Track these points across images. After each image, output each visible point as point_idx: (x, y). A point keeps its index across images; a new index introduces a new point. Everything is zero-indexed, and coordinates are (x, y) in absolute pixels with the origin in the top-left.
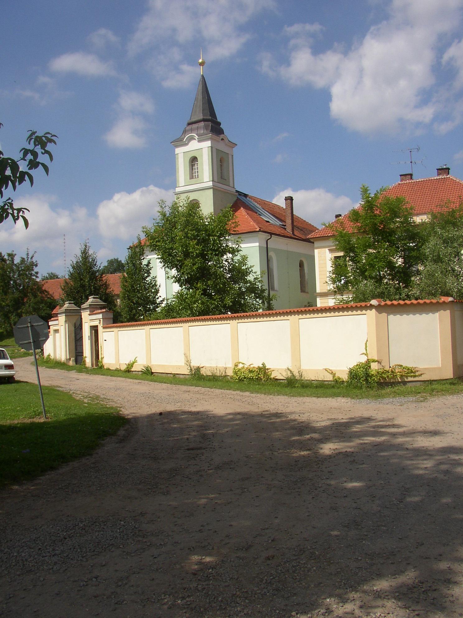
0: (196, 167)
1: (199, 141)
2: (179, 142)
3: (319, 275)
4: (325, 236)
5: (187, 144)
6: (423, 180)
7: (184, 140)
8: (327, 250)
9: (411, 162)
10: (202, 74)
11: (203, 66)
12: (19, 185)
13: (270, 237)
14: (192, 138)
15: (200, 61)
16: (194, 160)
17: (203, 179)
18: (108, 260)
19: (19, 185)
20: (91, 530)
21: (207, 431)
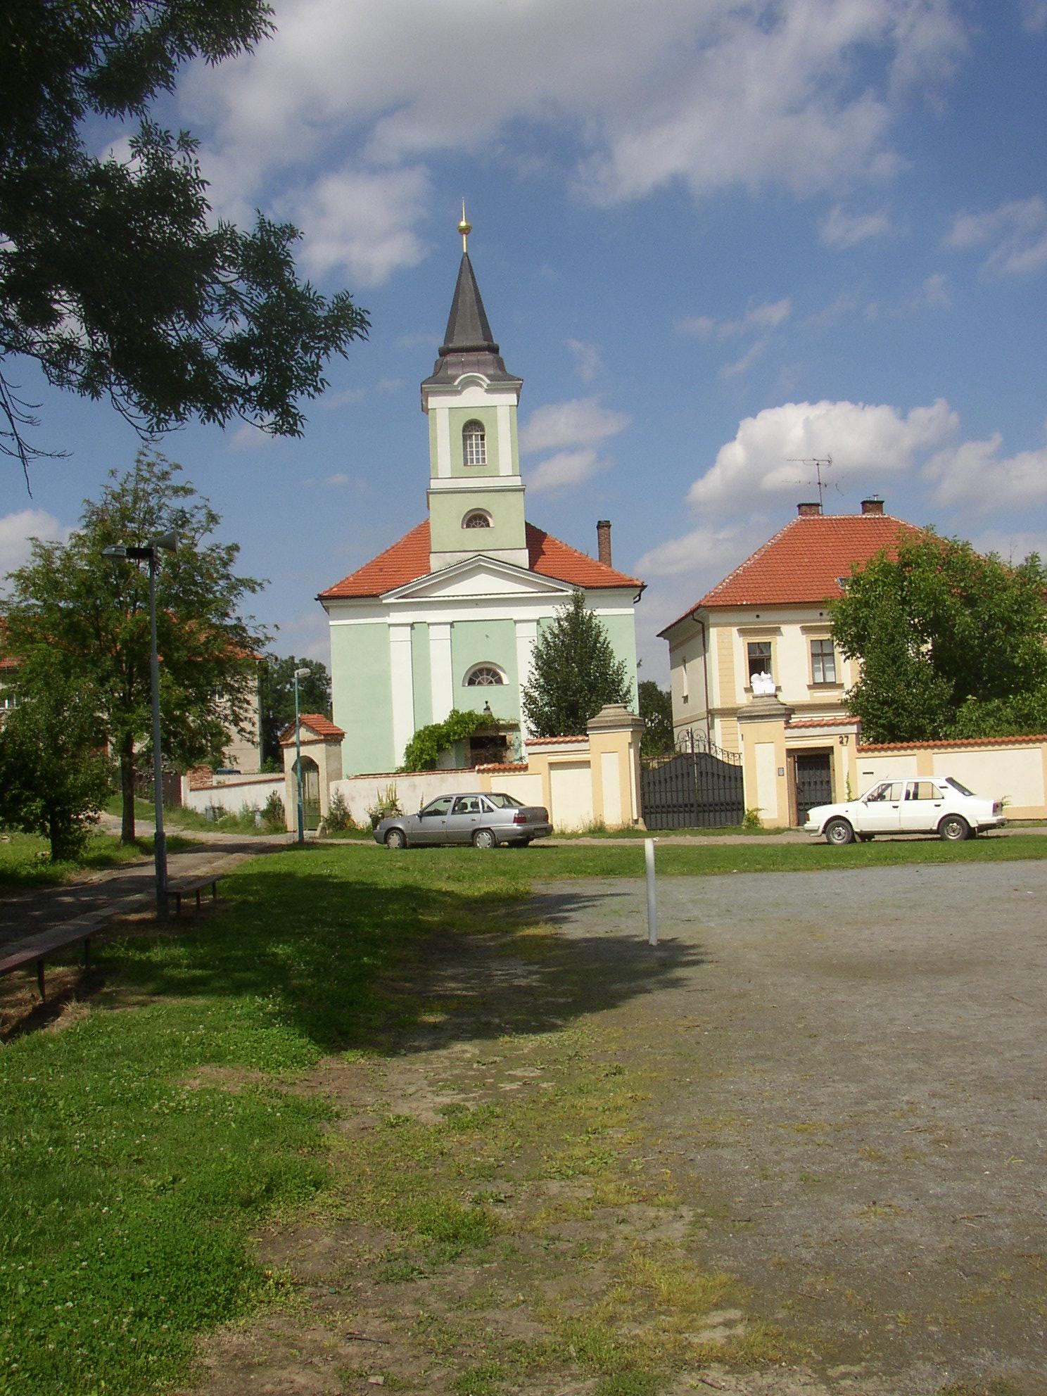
0: (474, 442)
1: (489, 390)
2: (440, 381)
3: (720, 669)
4: (737, 605)
5: (459, 393)
6: (842, 517)
7: (456, 383)
8: (734, 630)
9: (819, 483)
10: (465, 251)
11: (467, 234)
12: (672, 668)
13: (701, 625)
14: (473, 382)
15: (463, 224)
16: (473, 428)
17: (497, 469)
18: (629, 743)
19: (672, 668)
20: (480, 1332)
21: (62, 898)
